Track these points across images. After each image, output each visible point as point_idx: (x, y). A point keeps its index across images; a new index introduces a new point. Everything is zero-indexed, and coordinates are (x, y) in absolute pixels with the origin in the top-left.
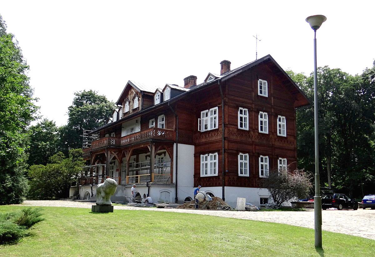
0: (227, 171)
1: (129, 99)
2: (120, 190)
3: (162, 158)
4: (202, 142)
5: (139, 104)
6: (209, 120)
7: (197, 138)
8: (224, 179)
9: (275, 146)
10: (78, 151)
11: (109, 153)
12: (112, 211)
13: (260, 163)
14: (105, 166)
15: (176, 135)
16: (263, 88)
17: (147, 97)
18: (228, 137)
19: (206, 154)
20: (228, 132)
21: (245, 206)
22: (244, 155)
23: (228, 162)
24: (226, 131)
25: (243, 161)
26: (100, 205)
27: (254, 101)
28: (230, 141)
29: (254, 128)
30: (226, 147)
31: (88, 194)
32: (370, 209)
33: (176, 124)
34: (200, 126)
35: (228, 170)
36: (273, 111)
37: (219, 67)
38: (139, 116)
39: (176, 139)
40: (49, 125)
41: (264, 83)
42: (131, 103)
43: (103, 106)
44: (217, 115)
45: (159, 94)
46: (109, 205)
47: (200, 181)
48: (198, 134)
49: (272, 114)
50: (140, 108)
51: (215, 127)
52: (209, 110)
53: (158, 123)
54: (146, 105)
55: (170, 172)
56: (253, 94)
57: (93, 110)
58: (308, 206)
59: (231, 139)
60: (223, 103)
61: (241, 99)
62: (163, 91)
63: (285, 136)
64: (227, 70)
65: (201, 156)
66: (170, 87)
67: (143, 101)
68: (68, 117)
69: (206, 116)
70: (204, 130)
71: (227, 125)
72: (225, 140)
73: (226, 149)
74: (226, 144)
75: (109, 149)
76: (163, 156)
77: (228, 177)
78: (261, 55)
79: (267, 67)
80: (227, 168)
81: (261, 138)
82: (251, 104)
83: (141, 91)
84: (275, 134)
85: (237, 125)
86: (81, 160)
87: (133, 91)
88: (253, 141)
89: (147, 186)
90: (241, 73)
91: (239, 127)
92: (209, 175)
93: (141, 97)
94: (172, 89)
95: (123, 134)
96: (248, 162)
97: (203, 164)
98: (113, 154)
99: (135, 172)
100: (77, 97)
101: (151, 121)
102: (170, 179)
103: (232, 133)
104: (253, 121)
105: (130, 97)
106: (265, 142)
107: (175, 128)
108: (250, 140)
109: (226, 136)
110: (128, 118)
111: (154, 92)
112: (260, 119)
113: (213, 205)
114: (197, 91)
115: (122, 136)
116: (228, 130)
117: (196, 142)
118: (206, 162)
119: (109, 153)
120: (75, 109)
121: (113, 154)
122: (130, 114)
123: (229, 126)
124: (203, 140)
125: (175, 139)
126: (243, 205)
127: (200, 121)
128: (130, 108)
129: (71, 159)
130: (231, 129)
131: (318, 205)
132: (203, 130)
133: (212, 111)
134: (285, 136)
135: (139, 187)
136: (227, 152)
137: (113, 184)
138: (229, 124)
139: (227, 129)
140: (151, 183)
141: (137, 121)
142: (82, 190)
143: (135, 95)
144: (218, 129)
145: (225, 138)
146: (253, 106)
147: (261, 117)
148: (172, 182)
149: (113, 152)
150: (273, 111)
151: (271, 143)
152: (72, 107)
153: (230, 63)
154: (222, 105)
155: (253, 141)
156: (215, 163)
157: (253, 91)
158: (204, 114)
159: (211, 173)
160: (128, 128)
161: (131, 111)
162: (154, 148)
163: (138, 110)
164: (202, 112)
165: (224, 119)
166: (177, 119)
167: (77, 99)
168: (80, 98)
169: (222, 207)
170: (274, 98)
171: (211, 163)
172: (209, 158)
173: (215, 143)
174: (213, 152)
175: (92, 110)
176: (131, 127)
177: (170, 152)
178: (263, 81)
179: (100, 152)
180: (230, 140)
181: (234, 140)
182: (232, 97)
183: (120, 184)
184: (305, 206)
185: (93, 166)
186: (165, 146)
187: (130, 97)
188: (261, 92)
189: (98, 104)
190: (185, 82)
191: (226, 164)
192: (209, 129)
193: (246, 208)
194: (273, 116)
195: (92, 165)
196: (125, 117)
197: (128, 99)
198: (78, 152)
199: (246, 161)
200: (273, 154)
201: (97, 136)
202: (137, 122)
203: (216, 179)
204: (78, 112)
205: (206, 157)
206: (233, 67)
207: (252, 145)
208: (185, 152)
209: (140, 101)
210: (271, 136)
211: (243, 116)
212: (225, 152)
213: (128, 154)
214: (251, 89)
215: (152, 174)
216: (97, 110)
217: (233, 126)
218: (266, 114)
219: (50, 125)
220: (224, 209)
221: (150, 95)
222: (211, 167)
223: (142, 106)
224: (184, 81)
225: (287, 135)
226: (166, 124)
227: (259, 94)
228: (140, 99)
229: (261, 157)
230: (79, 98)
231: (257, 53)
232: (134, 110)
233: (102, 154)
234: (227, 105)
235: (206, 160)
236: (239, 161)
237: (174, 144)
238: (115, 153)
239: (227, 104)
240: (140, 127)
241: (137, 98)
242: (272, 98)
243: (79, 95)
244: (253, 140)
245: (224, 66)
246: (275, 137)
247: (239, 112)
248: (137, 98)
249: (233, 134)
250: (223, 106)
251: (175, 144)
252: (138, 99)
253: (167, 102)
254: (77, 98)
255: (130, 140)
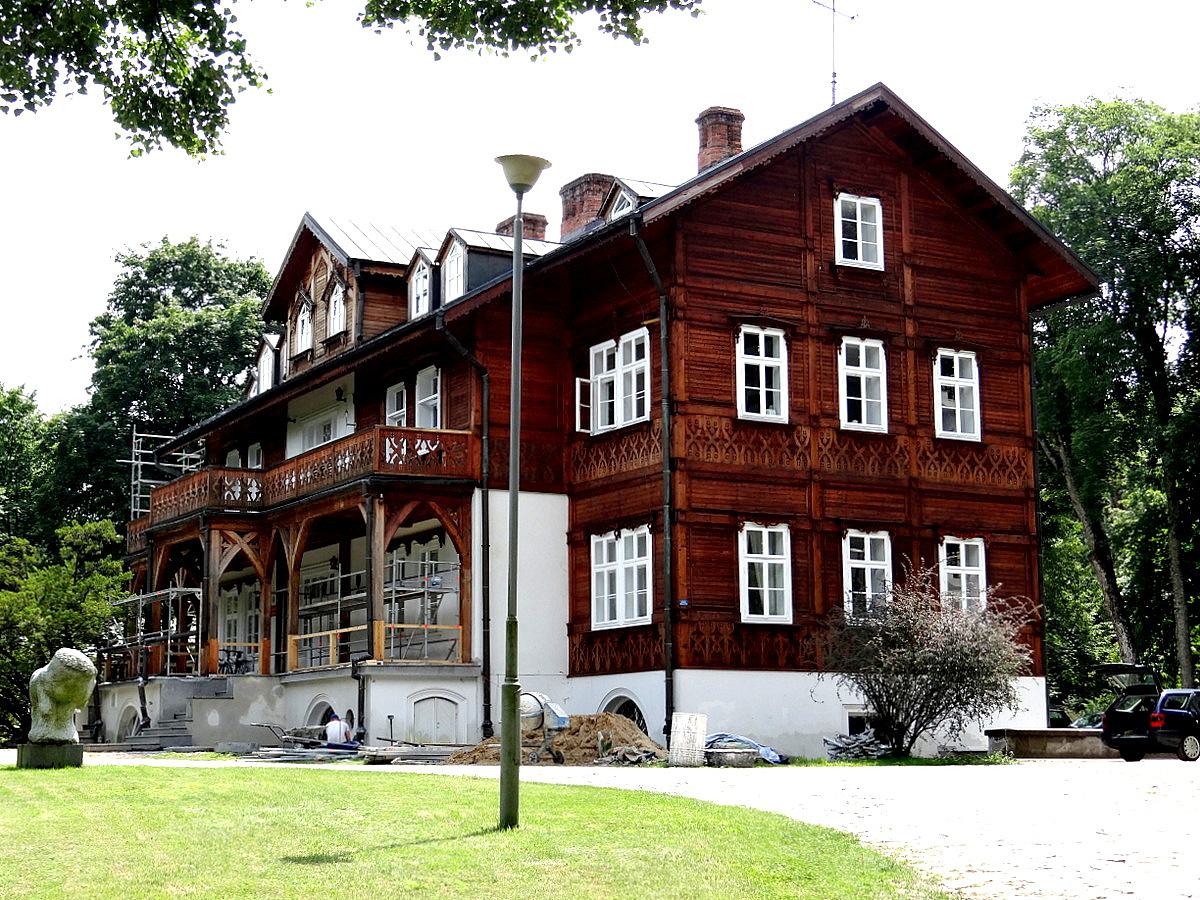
0: (683, 603)
1: (312, 297)
2: (257, 698)
3: (434, 556)
4: (593, 478)
5: (348, 317)
6: (619, 381)
7: (577, 463)
8: (674, 640)
9: (924, 487)
10: (97, 532)
11: (216, 537)
12: (78, 763)
13: (848, 564)
14: (200, 597)
15: (482, 455)
16: (863, 231)
17: (381, 283)
18: (689, 458)
19: (643, 524)
20: (688, 437)
21: (701, 743)
22: (765, 532)
23: (691, 561)
24: (680, 431)
25: (766, 562)
26: (36, 743)
27: (814, 294)
28: (695, 474)
29: (814, 411)
30: (680, 503)
31: (134, 718)
32: (1022, 745)
33: (482, 406)
34: (582, 409)
35: (688, 600)
36: (910, 330)
37: (694, 132)
38: (348, 371)
39: (482, 473)
40: (7, 408)
41: (867, 211)
42: (320, 313)
43: (244, 312)
44: (646, 364)
45: (427, 271)
46: (67, 742)
47: (594, 651)
48: (579, 446)
49: (906, 342)
50: (353, 336)
51: (641, 413)
52: (617, 342)
53: (418, 402)
54: (379, 319)
55: (458, 613)
56: (811, 261)
57: (201, 329)
58: (1066, 746)
59: (704, 462)
60: (663, 309)
61: (748, 288)
62: (441, 257)
63: (976, 436)
64: (727, 150)
65: (594, 539)
66: (463, 242)
67: (364, 302)
68: (90, 367)
69: (608, 364)
70: (600, 427)
71: (683, 403)
72: (673, 468)
73: (680, 510)
74: (681, 489)
75: (217, 523)
76: (435, 542)
77: (698, 626)
78: (852, 86)
79: (878, 140)
80: (682, 591)
81: (851, 453)
82: (801, 306)
83: (353, 262)
84: (921, 432)
85: (733, 405)
86: (115, 572)
87: (327, 260)
88: (811, 470)
89: (356, 677)
90: (738, 179)
91: (742, 413)
92: (621, 622)
93: (355, 287)
94: (473, 251)
95: (293, 449)
96: (785, 559)
97: (600, 575)
98: (235, 543)
99: (337, 617)
100: (130, 271)
101: (391, 393)
102: (459, 648)
103: (707, 439)
104: (814, 386)
105: (315, 284)
106: (870, 470)
107: (475, 426)
108: (797, 464)
109: (680, 451)
110: (305, 383)
111: (407, 263)
112: (844, 371)
113: (589, 745)
114: (561, 262)
115: (289, 456)
116: (690, 427)
117: (574, 479)
118: (611, 566)
119: (216, 537)
120: (120, 332)
121: (235, 543)
122: (318, 363)
123: (691, 409)
124: (600, 472)
125: (477, 472)
126: (692, 741)
127: (585, 388)
128: (315, 335)
129: (70, 567)
130: (702, 422)
131: (506, 708)
132: (599, 427)
133: (628, 345)
134: (976, 436)
135: (330, 681)
136: (681, 523)
137: (78, 669)
138: (693, 401)
139: (681, 421)
140: (369, 662)
141: (340, 394)
142: (113, 704)
143: (331, 277)
144: (648, 425)
145: (673, 463)
146: (811, 316)
147: (853, 360)
148: (467, 659)
149: (233, 535)
150: (910, 330)
151: (901, 475)
152: (105, 321)
153: (740, 118)
154: (661, 320)
155: (811, 470)
156: (642, 571)
157: (811, 250)
158: (599, 355)
159: (628, 614)
160: (310, 424)
161: (320, 351)
162: (380, 514)
163: (346, 341)
164: (593, 350)
165: (671, 379)
166: (483, 383)
167: (129, 284)
168: (143, 277)
169: (616, 754)
170: (917, 270)
171: (629, 571)
172: (620, 546)
173: (638, 485)
174: (633, 524)
175: (191, 330)
176: (322, 419)
177: (457, 528)
178: (859, 202)
179: (181, 534)
180: (699, 470)
181: (719, 470)
182: (706, 284)
183: (269, 673)
184: (1051, 746)
185: (158, 593)
186: (432, 503)
187: (315, 284)
188: (850, 251)
189: (226, 302)
190: (565, 202)
191: (682, 571)
192: (620, 422)
193: (708, 755)
194: (911, 354)
195: (157, 590)
196: (297, 374)
197: (308, 294)
198: (97, 537)
199: (776, 559)
200: (915, 522)
201: (198, 460)
202: (339, 399)
203: (645, 637)
204: (132, 342)
205: (612, 547)
206: (752, 136)
207: (802, 485)
208: (528, 525)
209: (353, 303)
210: (901, 441)
211: (762, 361)
212: (673, 522)
213: (291, 538)
214: (799, 242)
215: (376, 623)
216: (219, 333)
217: (710, 410)
218: (878, 344)
219: (11, 406)
220: (623, 761)
221: (395, 275)
222: (627, 391)
223: (361, 325)
224: (560, 200)
225: (984, 432)
226: (444, 407)
227: (840, 259)
228: (352, 293)
229: (851, 538)
230: (139, 278)
231: (834, 75)
232: (332, 343)
233: (193, 540)
234: (680, 320)
235: (612, 558)
236: (744, 559)
237: (471, 494)
238: (242, 535)
239: (680, 314)
240: (352, 421)
241: (339, 289)
242: (907, 273)
243: (137, 265)
244: (813, 461)
245: (710, 134)
246: (924, 443)
247: (740, 346)
248: (339, 289)
249: (711, 441)
250: (663, 324)
251: (477, 494)
252: (345, 293)
253: (457, 304)
254: (130, 276)
255: (298, 481)
